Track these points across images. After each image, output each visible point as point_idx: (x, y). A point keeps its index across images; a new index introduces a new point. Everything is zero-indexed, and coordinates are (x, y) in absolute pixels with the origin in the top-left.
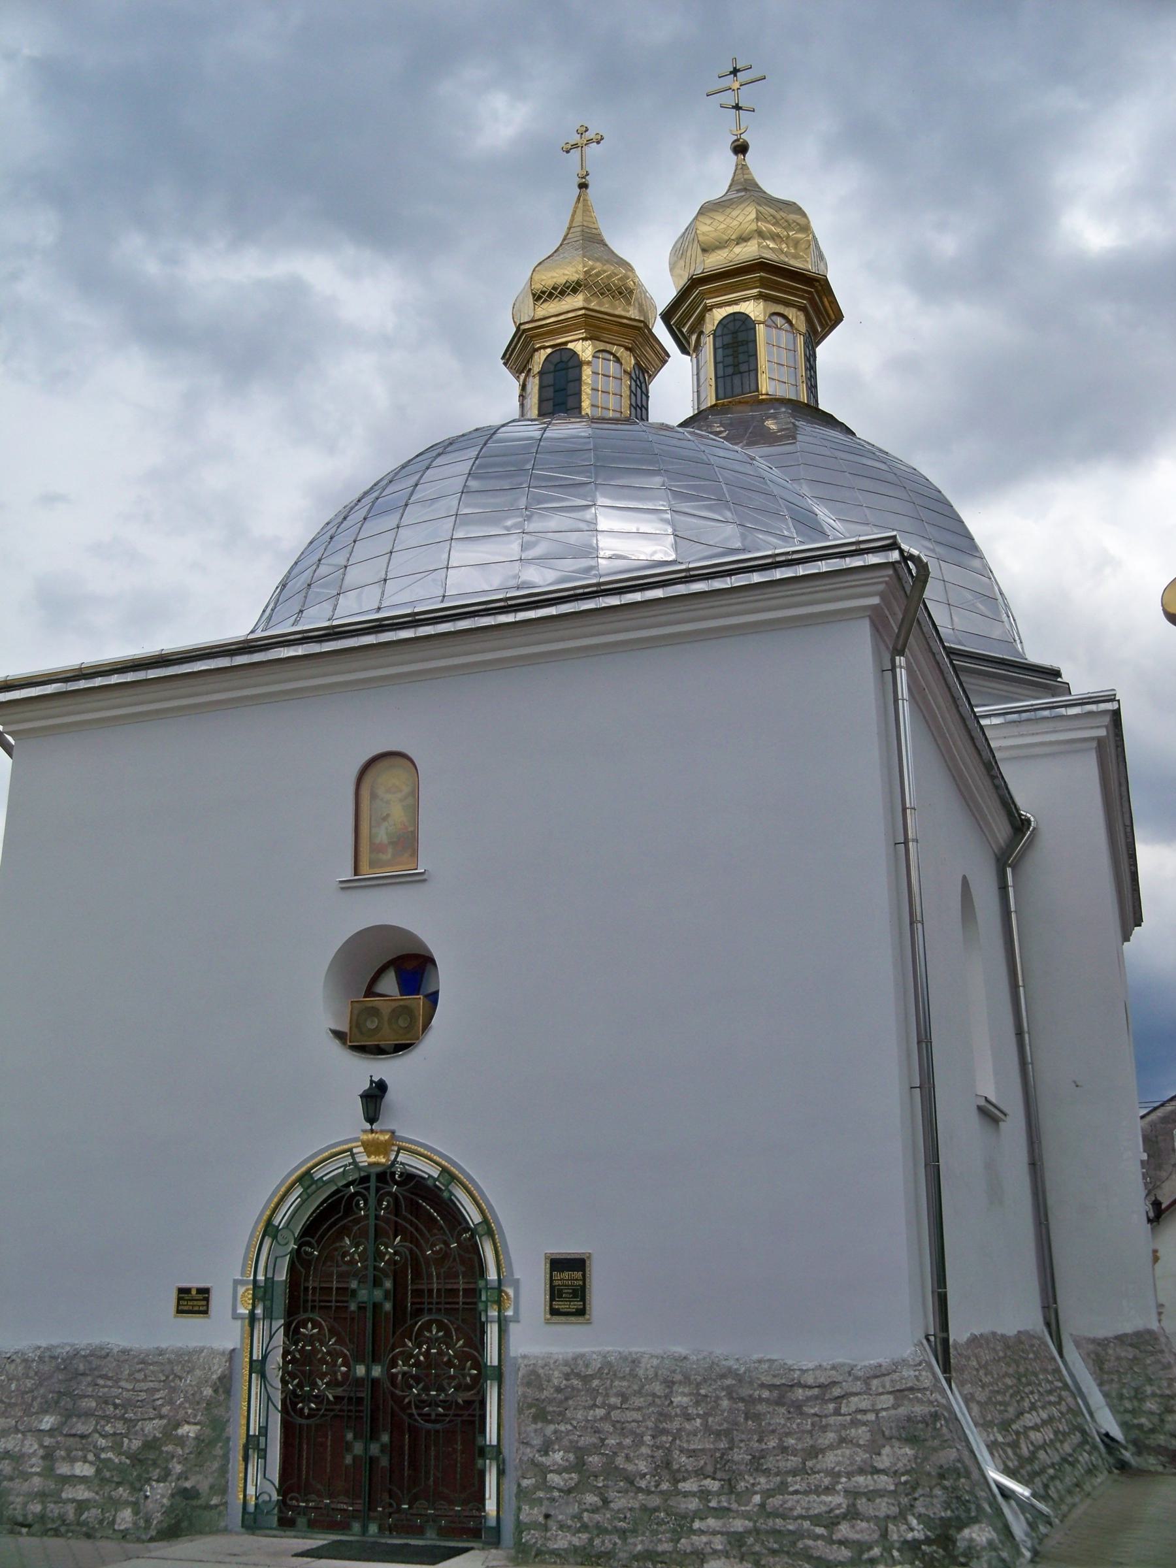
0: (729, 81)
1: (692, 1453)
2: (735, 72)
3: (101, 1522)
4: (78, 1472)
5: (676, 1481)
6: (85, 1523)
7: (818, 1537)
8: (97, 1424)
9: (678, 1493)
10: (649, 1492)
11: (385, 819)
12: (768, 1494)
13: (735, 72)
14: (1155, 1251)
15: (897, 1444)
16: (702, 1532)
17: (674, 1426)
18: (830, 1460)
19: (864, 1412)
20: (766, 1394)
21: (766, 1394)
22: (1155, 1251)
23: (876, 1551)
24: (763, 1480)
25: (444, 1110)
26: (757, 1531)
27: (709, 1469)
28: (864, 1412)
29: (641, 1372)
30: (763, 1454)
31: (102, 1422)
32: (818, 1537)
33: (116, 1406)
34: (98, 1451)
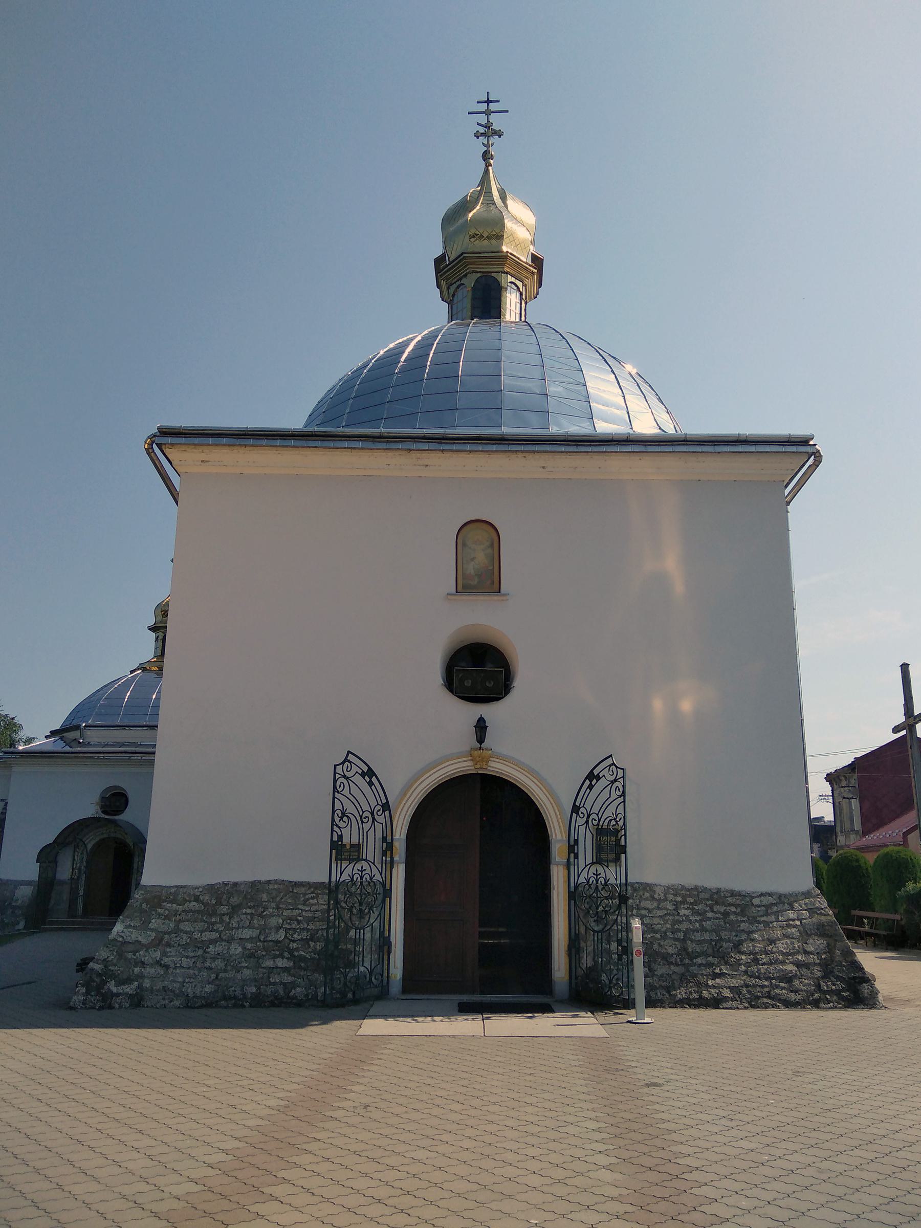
0: (484, 107)
1: (699, 942)
2: (488, 102)
3: (307, 995)
4: (280, 965)
5: (691, 959)
6: (295, 997)
7: (783, 988)
8: (286, 933)
9: (695, 965)
10: (677, 965)
11: (473, 559)
12: (748, 965)
13: (488, 102)
14: (481, 739)
15: (816, 938)
16: (714, 987)
17: (684, 926)
18: (781, 946)
19: (793, 920)
20: (733, 909)
21: (733, 909)
22: (481, 739)
23: (816, 995)
24: (743, 957)
25: (534, 748)
26: (747, 986)
27: (710, 951)
28: (793, 920)
29: (656, 896)
30: (740, 943)
31: (291, 932)
32: (783, 988)
33: (299, 922)
34: (291, 951)
